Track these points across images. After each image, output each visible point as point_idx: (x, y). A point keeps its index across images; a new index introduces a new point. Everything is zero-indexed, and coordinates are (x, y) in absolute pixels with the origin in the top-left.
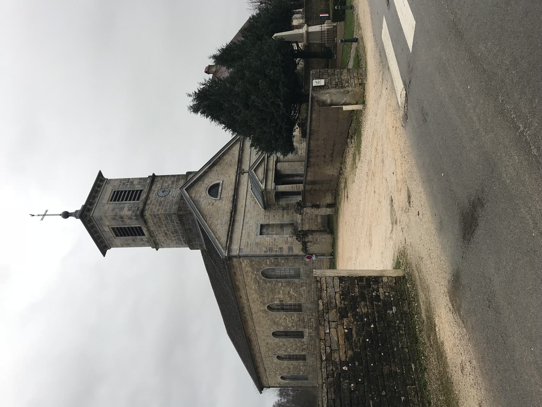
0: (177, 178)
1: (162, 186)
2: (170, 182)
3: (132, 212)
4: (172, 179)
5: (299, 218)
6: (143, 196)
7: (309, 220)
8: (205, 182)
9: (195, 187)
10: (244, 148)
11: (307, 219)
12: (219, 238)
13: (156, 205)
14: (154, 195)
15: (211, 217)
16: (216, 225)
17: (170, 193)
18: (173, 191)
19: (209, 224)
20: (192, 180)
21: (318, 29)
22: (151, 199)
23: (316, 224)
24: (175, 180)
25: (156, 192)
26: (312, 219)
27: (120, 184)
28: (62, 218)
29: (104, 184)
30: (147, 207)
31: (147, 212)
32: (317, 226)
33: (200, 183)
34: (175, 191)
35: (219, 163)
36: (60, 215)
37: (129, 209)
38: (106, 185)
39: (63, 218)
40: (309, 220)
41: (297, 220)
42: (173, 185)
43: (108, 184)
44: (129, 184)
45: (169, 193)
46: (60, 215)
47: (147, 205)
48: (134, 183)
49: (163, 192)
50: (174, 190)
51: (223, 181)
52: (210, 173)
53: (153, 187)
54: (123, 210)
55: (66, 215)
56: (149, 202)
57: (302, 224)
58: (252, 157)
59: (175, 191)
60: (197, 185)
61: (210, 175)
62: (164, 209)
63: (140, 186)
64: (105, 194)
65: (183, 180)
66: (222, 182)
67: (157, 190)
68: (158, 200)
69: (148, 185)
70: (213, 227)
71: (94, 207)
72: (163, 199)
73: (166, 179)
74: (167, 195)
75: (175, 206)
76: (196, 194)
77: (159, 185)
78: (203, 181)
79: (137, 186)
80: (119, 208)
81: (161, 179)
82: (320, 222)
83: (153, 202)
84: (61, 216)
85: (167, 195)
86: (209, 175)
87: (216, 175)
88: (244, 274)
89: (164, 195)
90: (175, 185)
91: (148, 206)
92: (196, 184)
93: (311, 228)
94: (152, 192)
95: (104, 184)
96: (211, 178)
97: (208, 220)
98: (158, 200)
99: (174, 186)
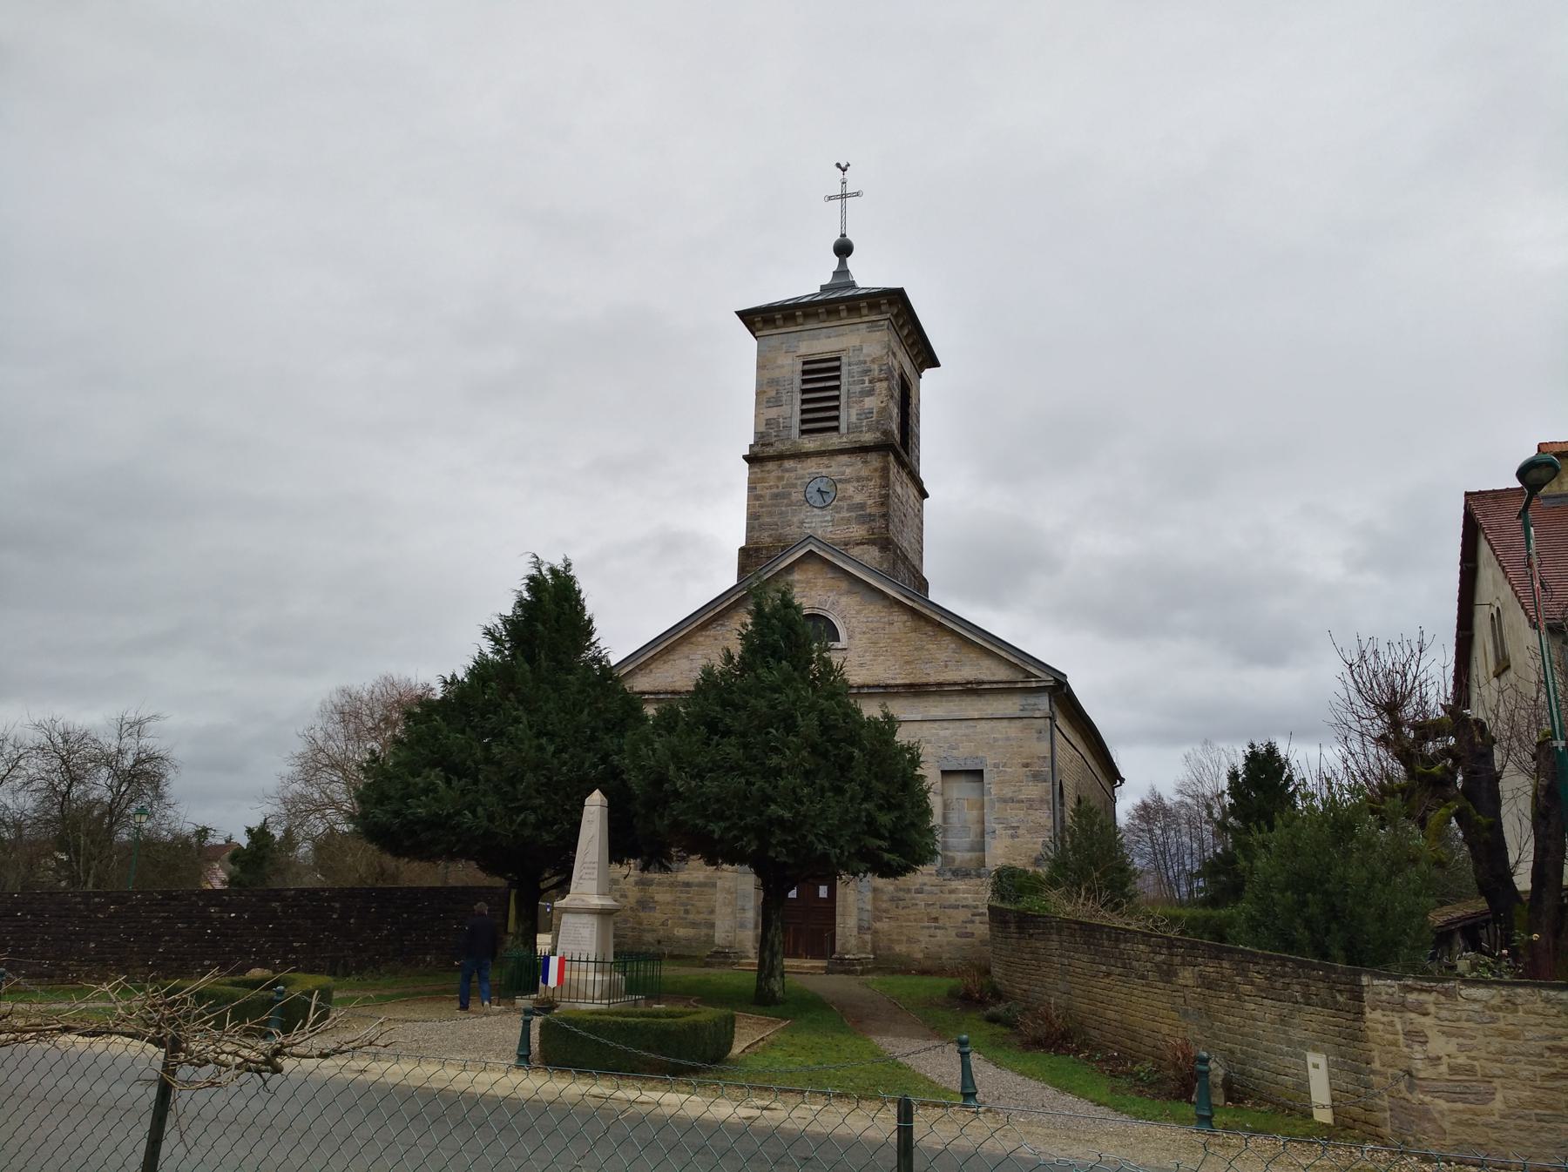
0: (874, 515)
1: (848, 481)
2: (858, 499)
3: (761, 433)
4: (870, 502)
5: (695, 875)
6: (810, 444)
7: (682, 904)
8: (844, 600)
9: (827, 574)
10: (987, 697)
11: (688, 898)
12: (648, 671)
13: (778, 487)
14: (813, 470)
15: (716, 639)
16: (688, 657)
17: (816, 511)
18: (826, 515)
19: (694, 639)
20: (844, 562)
21: (564, 946)
22: (799, 466)
23: (670, 922)
24: (868, 511)
25: (824, 471)
26: (687, 912)
27: (868, 359)
28: (835, 240)
29: (866, 319)
30: (771, 466)
31: (756, 472)
32: (663, 924)
33: (844, 585)
34: (825, 521)
35: (923, 623)
36: (843, 235)
37: (773, 421)
38: (864, 325)
39: (834, 242)
40: (682, 904)
41: (687, 872)
42: (847, 510)
43: (868, 327)
44: (867, 384)
45: (816, 507)
46: (843, 235)
47: (779, 462)
48: (867, 399)
49: (819, 490)
50: (829, 518)
51: (845, 649)
52: (880, 607)
53: (844, 459)
54: (769, 407)
55: (843, 249)
56: (789, 464)
57: (672, 885)
58: (945, 724)
59: (825, 521)
60: (833, 578)
61: (872, 607)
62: (763, 512)
63: (854, 419)
64: (829, 337)
65: (864, 533)
66: (840, 647)
67: (830, 472)
68: (794, 486)
69: (855, 439)
70: (685, 649)
71: (784, 330)
72: (797, 496)
73: (872, 483)
74: (810, 505)
75: (770, 536)
76: (802, 583)
77: (848, 471)
78: (849, 592)
79: (854, 412)
80: (777, 393)
81: (876, 470)
82: (676, 932)
83: (787, 475)
84: (839, 237)
85: (810, 505)
86: (871, 604)
87: (871, 626)
88: (1458, 1013)
89: (808, 496)
90: (848, 515)
91: (775, 467)
92: (837, 575)
93: (658, 907)
94: (825, 460)
95: (866, 319)
96: (858, 612)
97: (708, 633)
98: (794, 486)
99: (845, 514)
